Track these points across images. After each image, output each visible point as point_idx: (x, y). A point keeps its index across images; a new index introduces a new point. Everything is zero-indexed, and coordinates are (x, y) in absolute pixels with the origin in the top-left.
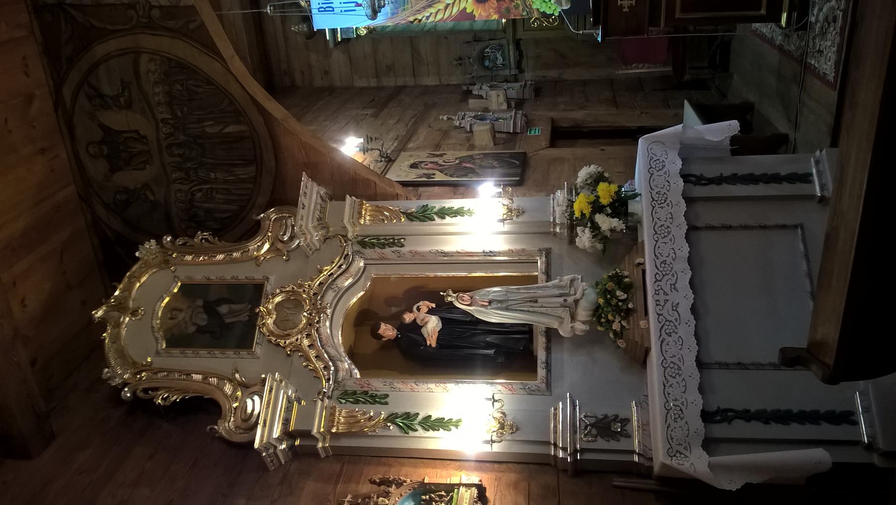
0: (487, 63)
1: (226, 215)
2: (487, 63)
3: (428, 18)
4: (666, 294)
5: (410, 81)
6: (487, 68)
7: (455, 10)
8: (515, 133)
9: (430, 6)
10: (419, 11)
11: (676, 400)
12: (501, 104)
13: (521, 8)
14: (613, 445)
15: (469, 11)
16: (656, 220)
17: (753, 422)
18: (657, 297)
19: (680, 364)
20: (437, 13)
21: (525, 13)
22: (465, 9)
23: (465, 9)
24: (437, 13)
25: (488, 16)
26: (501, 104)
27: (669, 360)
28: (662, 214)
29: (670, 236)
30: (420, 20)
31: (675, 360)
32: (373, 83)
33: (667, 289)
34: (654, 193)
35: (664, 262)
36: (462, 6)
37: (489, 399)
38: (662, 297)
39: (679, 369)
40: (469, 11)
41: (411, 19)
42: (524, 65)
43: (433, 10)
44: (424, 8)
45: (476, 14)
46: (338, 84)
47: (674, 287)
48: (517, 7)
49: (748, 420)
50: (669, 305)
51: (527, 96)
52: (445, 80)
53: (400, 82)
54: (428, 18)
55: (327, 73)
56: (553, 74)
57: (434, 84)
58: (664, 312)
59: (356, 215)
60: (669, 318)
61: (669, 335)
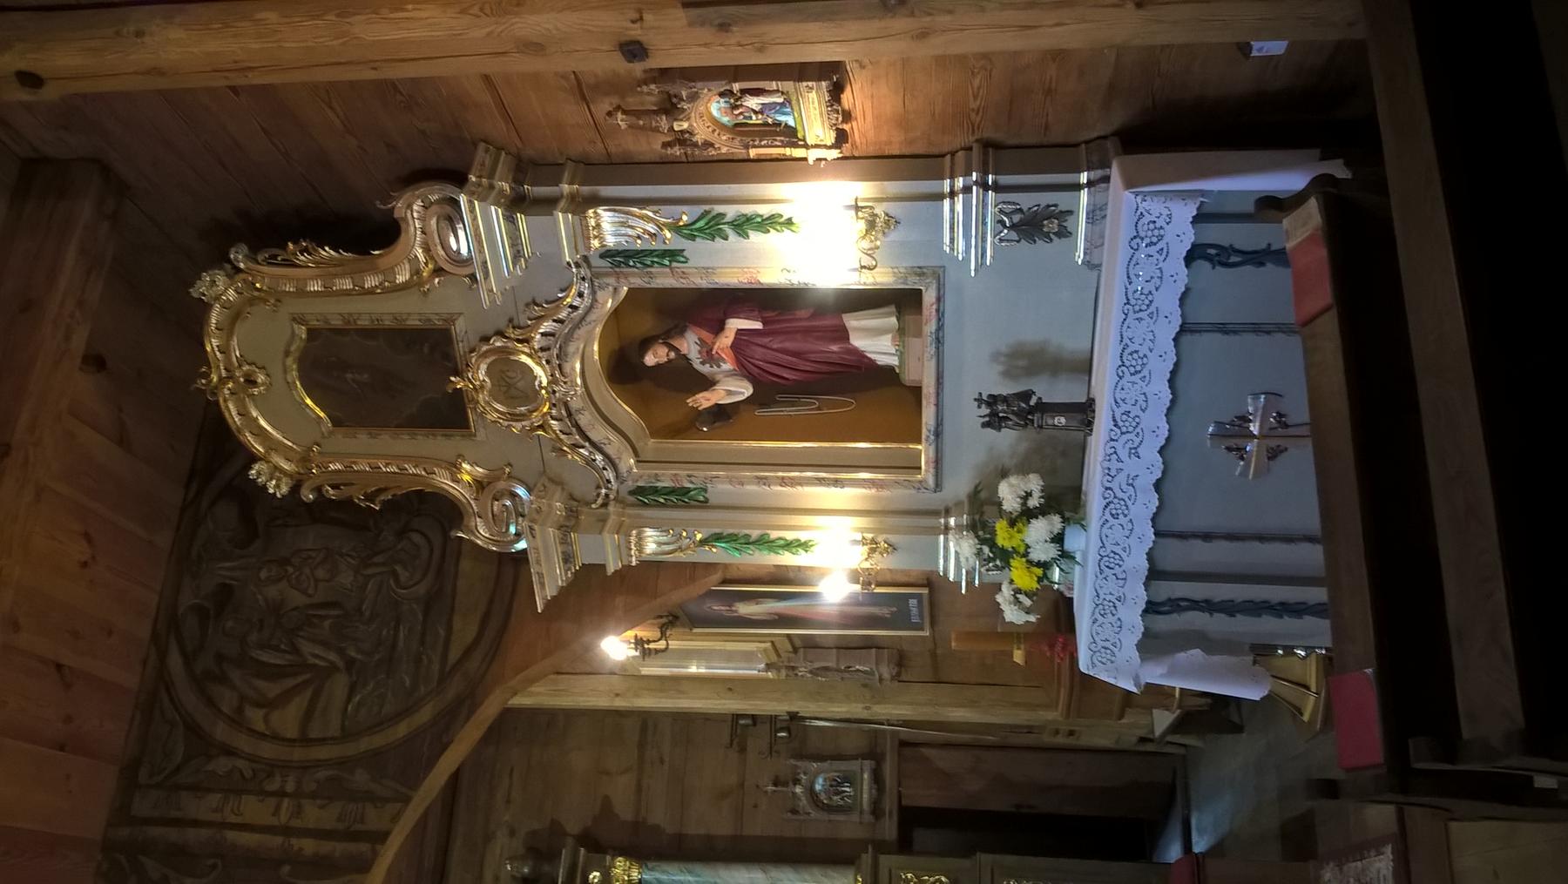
1: (322, 663)
4: (1119, 460)
14: (1027, 201)
16: (1126, 341)
17: (1239, 617)
18: (1106, 464)
19: (1124, 555)
27: (1109, 548)
28: (1139, 331)
31: (1118, 549)
35: (1127, 413)
37: (849, 207)
38: (1114, 465)
39: (1113, 654)
47: (1134, 452)
49: (1226, 333)
57: (882, 360)
58: (1114, 485)
59: (624, 551)
60: (1120, 495)
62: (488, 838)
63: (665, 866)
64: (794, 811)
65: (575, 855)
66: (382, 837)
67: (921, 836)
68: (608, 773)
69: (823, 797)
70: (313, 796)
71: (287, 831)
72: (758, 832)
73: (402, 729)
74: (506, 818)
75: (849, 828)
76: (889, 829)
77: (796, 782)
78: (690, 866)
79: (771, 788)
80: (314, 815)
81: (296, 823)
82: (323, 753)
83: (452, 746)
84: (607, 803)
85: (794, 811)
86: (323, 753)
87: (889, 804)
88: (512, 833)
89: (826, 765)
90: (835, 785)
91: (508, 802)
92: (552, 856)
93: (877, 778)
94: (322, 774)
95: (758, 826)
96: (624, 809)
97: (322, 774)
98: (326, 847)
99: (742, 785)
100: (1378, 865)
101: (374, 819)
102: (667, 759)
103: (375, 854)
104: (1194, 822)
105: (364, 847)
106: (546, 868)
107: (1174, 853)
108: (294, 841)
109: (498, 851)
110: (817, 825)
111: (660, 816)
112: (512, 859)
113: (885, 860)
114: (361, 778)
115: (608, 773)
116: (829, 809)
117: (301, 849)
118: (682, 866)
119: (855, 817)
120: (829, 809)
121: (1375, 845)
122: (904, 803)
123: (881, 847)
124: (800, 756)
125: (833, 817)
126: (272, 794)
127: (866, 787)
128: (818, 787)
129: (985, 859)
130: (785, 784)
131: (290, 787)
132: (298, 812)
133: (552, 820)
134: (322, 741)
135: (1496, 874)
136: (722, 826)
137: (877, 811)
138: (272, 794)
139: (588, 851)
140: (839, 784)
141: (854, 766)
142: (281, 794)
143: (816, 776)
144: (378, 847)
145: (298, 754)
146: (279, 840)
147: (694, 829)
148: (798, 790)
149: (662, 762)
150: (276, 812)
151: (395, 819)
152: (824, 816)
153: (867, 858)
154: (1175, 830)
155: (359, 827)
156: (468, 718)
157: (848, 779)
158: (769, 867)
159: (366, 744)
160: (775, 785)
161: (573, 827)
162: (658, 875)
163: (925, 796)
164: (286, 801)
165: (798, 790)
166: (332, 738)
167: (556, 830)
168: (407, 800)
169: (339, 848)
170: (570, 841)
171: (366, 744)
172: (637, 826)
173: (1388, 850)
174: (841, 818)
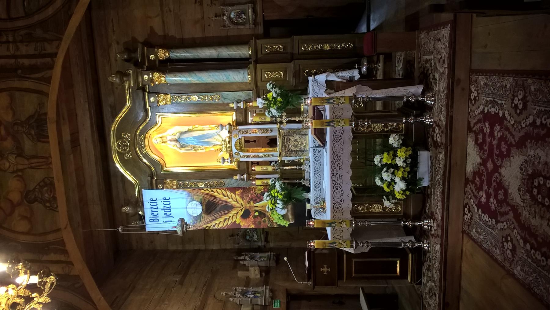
0: (248, 238)
2: (248, 238)
3: (214, 226)
5: (203, 247)
6: (248, 240)
7: (230, 222)
8: (265, 305)
9: (215, 220)
10: (209, 222)
11: (338, 236)
12: (257, 275)
13: (267, 222)
15: (237, 223)
20: (219, 223)
21: (269, 225)
22: (235, 221)
23: (235, 221)
24: (219, 223)
25: (248, 226)
26: (257, 275)
27: (336, 200)
29: (342, 140)
30: (210, 227)
31: (339, 201)
32: (180, 248)
33: (338, 169)
34: (335, 155)
36: (234, 220)
40: (237, 223)
41: (205, 226)
42: (269, 239)
43: (217, 222)
44: (212, 220)
45: (242, 224)
46: (159, 248)
48: (265, 221)
50: (338, 175)
51: (271, 265)
52: (223, 247)
53: (197, 247)
54: (214, 226)
55: (152, 242)
56: (286, 244)
61: (337, 208)
62: (110, 46)
63: (178, 51)
64: (224, 26)
65: (143, 49)
66: (54, 55)
67: (274, 31)
68: (150, 18)
69: (234, 20)
70: (21, 42)
71: (15, 57)
72: (211, 35)
73: (50, 11)
74: (114, 38)
75: (246, 30)
76: (260, 30)
77: (224, 15)
78: (187, 50)
79: (214, 18)
80: (24, 49)
81: (19, 53)
82: (20, 23)
83: (74, 16)
84: (152, 28)
85: (224, 26)
86: (20, 23)
87: (260, 20)
88: (118, 43)
89: (234, 7)
90: (238, 15)
91: (114, 31)
92: (135, 51)
93: (254, 10)
94: (22, 32)
95: (213, 32)
96: (159, 31)
97: (22, 32)
98: (33, 61)
99: (203, 18)
100: (443, 32)
101: (49, 48)
102: (172, 10)
103: (54, 62)
104: (371, 17)
105: (48, 60)
106: (133, 55)
107: (363, 29)
108: (19, 60)
109: (114, 51)
110: (233, 31)
111: (173, 32)
112: (120, 53)
113: (259, 41)
114: (39, 32)
115: (150, 18)
116: (237, 24)
117: (23, 63)
118: (182, 50)
119: (247, 27)
120: (237, 24)
121: (444, 25)
122: (266, 19)
123: (258, 37)
124: (224, 5)
125: (239, 27)
126: (4, 43)
127: (250, 15)
128: (232, 16)
129: (296, 38)
130: (220, 16)
131: (11, 39)
132: (18, 49)
133: (132, 37)
134: (18, 19)
135: (489, 34)
136: (198, 34)
137: (255, 23)
138: (4, 43)
139: (148, 48)
140: (241, 14)
141: (245, 6)
142: (8, 42)
143: (231, 13)
144: (54, 59)
145: (9, 25)
146: (12, 61)
147: (186, 36)
148: (225, 18)
149: (171, 11)
150: (8, 50)
151: (58, 47)
152: (236, 27)
153: (252, 42)
154: (365, 19)
155: (43, 52)
156: (77, 4)
157: (243, 12)
158: (217, 48)
159: (37, 18)
160: (216, 17)
161: (141, 39)
162: (175, 54)
163: (273, 16)
164: (11, 45)
165: (225, 18)
166: (22, 17)
167: (135, 40)
168: (61, 39)
169: (39, 61)
170: (140, 45)
171: (37, 18)
172: (165, 36)
173: (449, 26)
174: (242, 27)
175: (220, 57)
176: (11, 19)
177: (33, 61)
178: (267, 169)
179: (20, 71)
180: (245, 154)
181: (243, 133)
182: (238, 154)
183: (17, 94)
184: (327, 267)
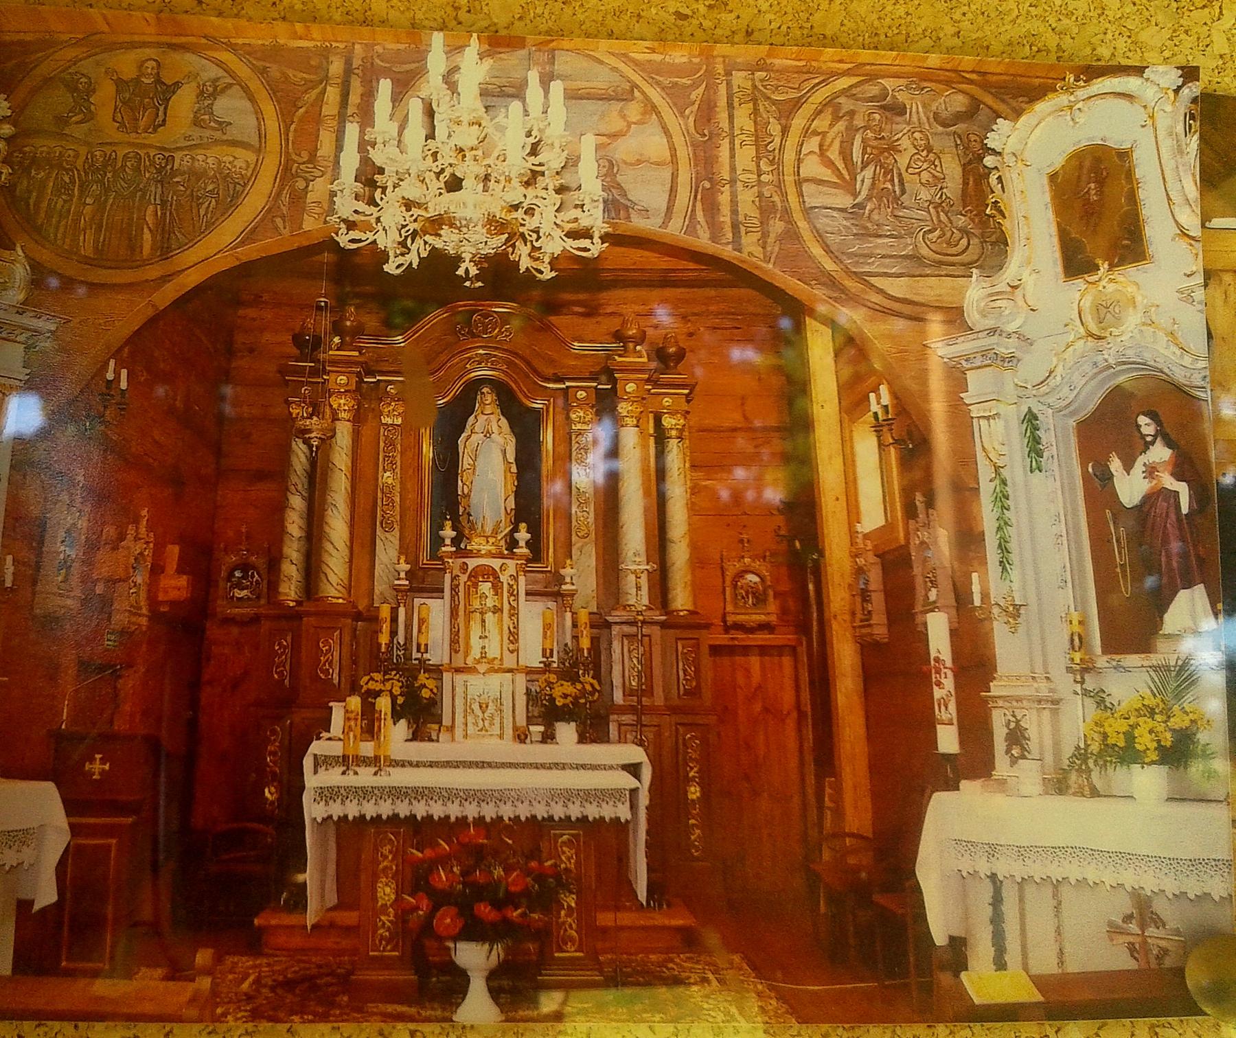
0: (238, 574)
6: (231, 575)
70: (760, 195)
80: (747, 199)
86: (793, 199)
93: (764, 627)
94: (776, 198)
98: (726, 210)
114: (777, 226)
134: (801, 194)
155: (743, 229)
175: (305, 515)
176: (799, 183)
177: (726, 210)
178: (932, 607)
179: (707, 185)
180: (461, 588)
181: (511, 586)
182: (464, 567)
183: (667, 174)
184: (103, 772)
